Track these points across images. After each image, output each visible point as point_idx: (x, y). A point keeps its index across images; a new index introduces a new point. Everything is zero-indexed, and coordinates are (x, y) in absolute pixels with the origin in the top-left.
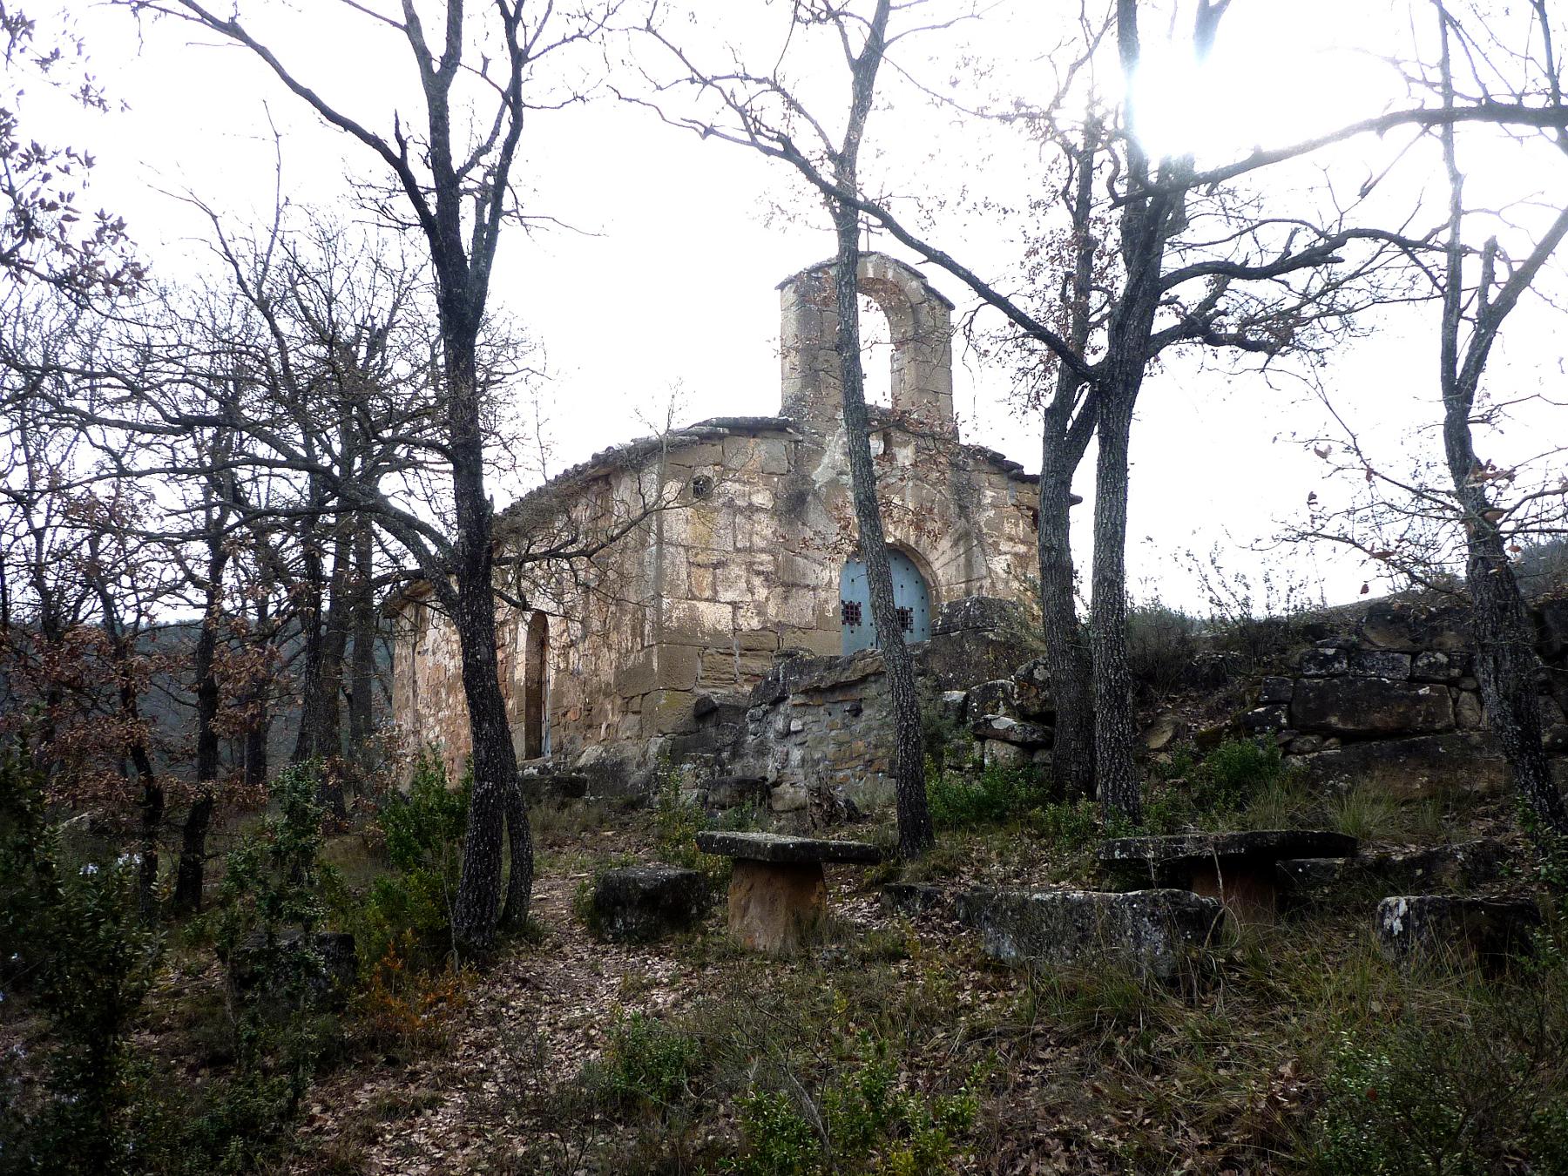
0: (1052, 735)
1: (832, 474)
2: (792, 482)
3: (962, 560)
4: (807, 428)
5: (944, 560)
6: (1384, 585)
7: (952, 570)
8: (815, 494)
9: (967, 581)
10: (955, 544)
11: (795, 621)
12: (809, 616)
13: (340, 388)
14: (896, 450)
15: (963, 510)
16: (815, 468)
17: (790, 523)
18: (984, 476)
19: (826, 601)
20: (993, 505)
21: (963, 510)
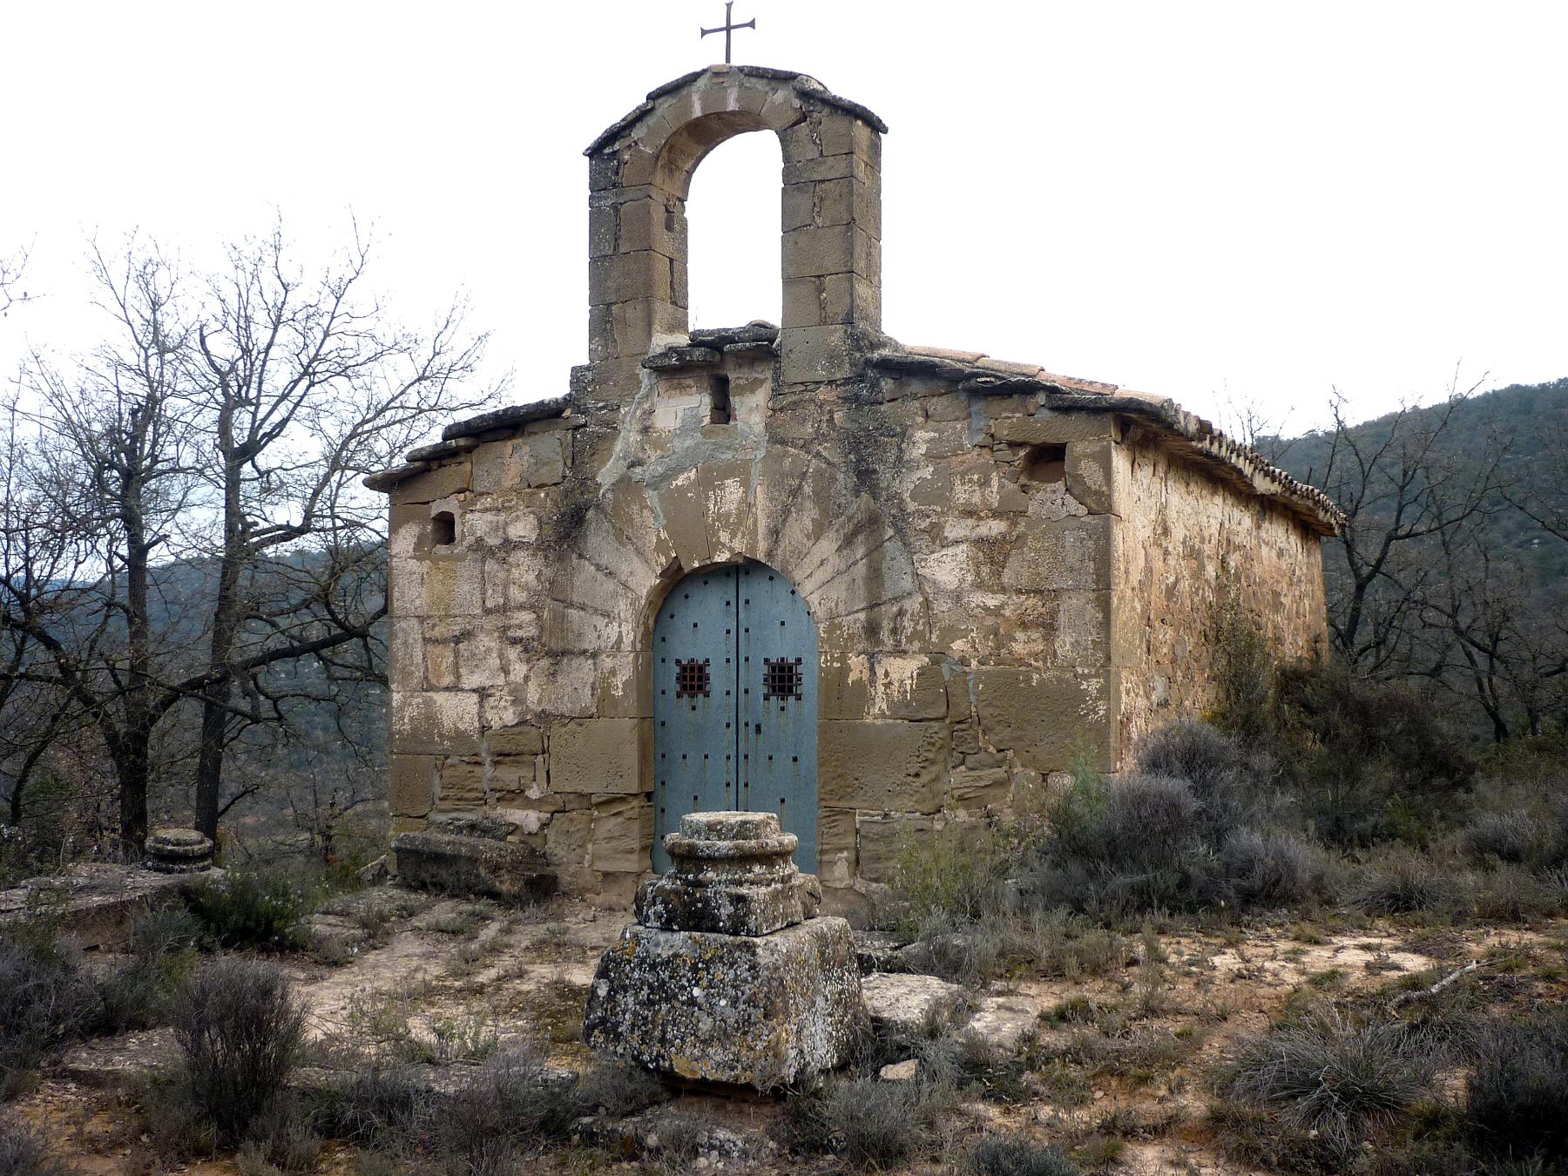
3: (861, 569)
4: (591, 403)
5: (822, 575)
7: (838, 592)
10: (848, 541)
11: (566, 708)
12: (586, 699)
14: (735, 400)
15: (865, 477)
16: (604, 463)
17: (561, 559)
20: (930, 456)
21: (865, 477)
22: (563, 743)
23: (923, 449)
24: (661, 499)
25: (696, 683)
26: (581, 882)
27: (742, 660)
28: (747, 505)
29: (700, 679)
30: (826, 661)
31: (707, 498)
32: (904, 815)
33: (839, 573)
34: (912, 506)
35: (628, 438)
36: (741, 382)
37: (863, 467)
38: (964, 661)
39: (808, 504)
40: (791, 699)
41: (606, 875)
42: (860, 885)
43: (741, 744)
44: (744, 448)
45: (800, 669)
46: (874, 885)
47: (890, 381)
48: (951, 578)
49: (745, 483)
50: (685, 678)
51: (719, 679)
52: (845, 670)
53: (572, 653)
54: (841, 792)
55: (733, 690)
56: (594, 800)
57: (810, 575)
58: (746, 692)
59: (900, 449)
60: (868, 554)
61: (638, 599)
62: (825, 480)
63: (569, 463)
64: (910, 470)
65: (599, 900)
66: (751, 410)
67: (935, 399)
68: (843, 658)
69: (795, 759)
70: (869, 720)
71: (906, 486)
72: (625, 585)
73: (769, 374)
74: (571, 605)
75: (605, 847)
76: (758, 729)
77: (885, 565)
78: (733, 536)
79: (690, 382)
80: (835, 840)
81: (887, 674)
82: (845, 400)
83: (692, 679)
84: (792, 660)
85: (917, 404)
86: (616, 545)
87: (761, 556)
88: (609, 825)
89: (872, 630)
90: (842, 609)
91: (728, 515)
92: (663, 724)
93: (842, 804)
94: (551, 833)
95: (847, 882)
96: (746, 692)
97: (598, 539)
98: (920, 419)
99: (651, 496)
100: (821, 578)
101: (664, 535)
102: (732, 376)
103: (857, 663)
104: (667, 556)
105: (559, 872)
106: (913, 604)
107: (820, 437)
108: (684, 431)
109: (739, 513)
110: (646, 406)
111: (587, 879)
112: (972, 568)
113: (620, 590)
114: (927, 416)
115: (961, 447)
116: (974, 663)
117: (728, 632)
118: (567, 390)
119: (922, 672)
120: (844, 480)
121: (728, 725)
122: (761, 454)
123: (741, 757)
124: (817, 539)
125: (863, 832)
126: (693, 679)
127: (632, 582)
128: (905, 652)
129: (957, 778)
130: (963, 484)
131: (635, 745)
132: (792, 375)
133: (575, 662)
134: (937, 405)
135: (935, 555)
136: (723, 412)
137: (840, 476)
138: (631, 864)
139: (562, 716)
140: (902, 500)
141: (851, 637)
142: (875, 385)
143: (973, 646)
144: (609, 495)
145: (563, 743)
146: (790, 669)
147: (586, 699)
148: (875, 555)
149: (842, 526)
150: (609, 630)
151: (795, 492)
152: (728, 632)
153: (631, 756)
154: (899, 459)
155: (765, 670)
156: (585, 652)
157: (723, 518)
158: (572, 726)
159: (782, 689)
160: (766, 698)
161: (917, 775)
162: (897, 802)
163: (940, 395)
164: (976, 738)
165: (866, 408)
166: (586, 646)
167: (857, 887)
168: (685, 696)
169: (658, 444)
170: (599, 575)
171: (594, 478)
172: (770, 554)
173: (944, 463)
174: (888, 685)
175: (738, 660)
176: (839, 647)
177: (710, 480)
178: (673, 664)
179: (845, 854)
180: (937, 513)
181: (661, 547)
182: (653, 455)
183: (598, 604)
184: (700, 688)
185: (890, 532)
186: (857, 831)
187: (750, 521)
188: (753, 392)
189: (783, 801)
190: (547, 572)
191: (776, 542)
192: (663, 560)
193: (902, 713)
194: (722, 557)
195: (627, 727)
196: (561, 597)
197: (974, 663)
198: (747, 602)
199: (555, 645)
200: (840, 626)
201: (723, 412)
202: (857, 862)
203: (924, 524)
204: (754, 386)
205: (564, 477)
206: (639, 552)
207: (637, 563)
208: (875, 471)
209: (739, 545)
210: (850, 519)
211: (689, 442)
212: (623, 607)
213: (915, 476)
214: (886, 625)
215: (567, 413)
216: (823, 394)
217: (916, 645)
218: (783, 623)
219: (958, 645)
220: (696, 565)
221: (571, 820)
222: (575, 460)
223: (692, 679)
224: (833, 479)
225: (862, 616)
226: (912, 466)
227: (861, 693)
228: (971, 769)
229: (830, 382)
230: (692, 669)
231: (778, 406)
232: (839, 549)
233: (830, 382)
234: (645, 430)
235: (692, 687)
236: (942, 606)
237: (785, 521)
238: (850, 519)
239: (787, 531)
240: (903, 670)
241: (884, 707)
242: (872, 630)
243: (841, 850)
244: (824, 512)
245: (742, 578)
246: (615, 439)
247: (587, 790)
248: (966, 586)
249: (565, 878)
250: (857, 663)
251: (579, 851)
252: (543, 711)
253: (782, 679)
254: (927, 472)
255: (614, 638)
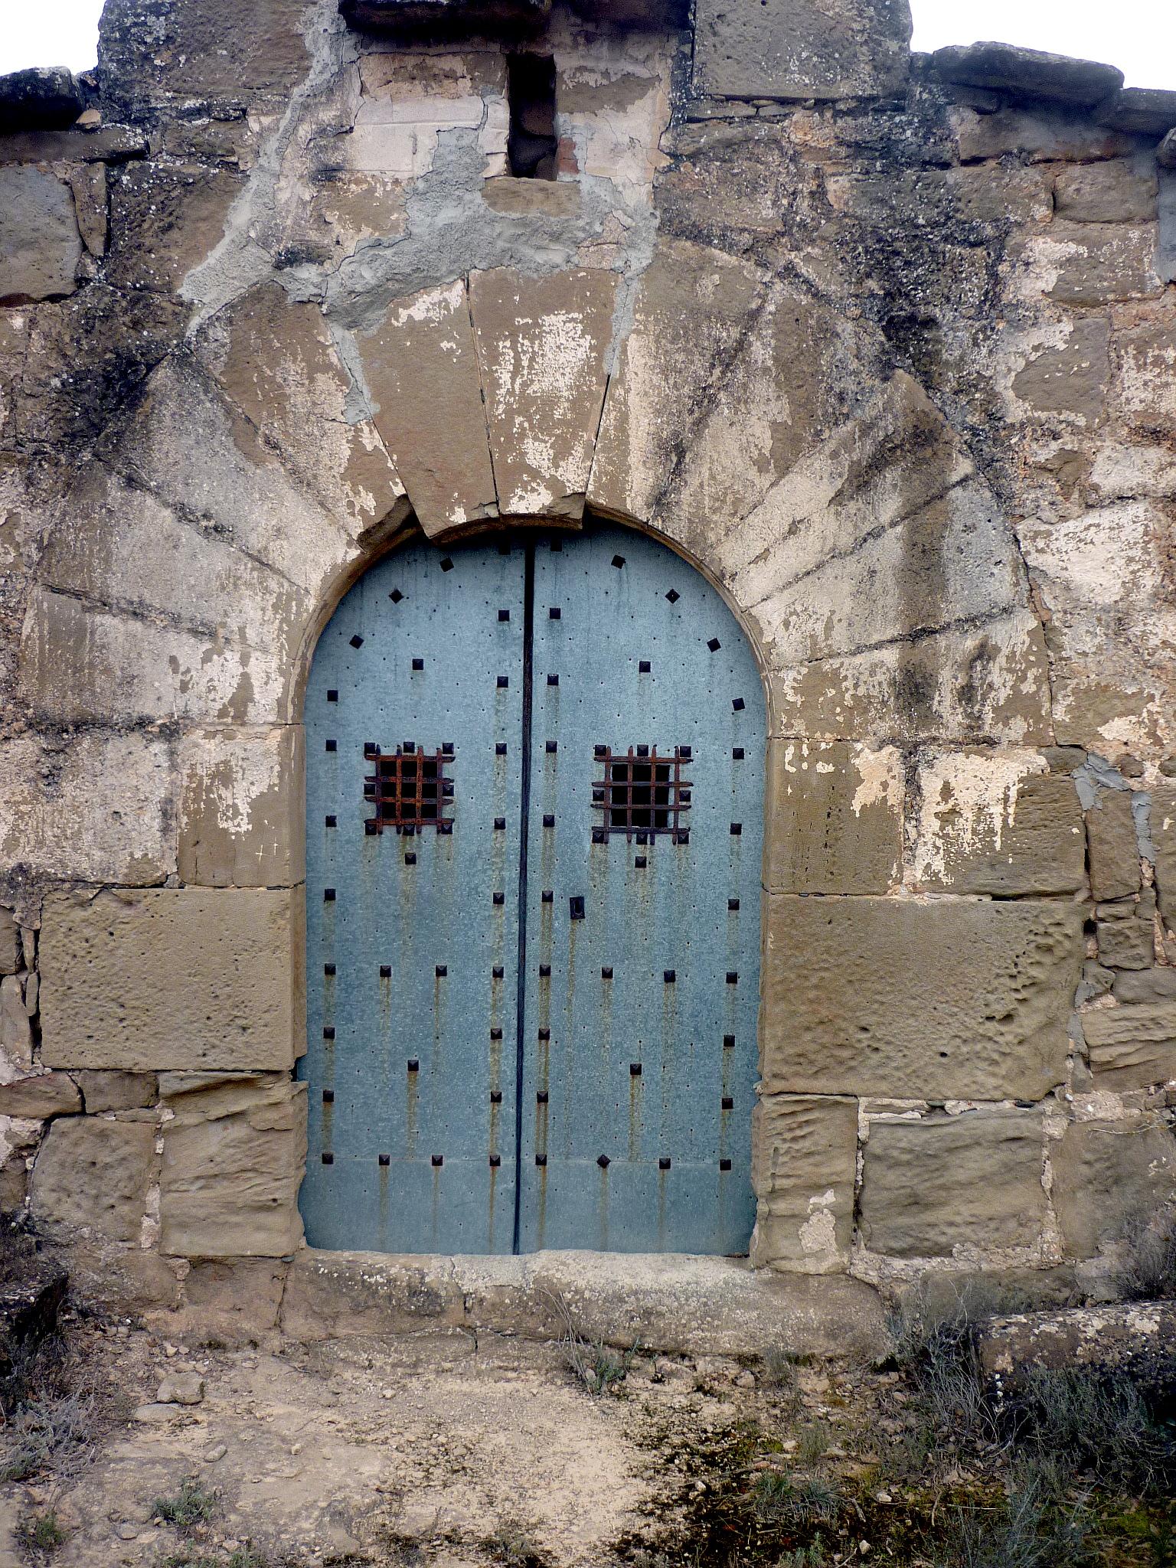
0: (278, 267)
1: (257, 265)
2: (89, 323)
3: (891, 549)
4: (161, 97)
5: (792, 557)
6: (151, 386)
7: (834, 597)
8: (184, 360)
9: (914, 636)
10: (861, 482)
11: (87, 861)
12: (147, 840)
13: (132, 363)
14: (570, 123)
15: (905, 332)
16: (197, 253)
17: (73, 487)
18: (1030, 177)
19: (224, 775)
20: (1069, 299)
21: (905, 332)
22: (79, 947)
23: (1049, 280)
24: (366, 349)
25: (418, 801)
26: (133, 1284)
27: (538, 751)
28: (601, 382)
29: (429, 791)
30: (799, 758)
31: (494, 357)
32: (979, 1104)
33: (836, 554)
34: (1016, 411)
35: (274, 189)
36: (591, 79)
37: (901, 309)
38: (1128, 766)
39: (763, 388)
40: (664, 841)
41: (199, 1263)
42: (865, 1265)
43: (533, 945)
44: (597, 240)
45: (687, 773)
46: (899, 1264)
47: (972, 117)
48: (1104, 578)
49: (599, 328)
50: (389, 790)
51: (477, 791)
52: (845, 781)
53: (104, 724)
54: (821, 1059)
55: (513, 818)
56: (168, 1085)
57: (764, 556)
58: (549, 822)
59: (994, 277)
60: (910, 514)
61: (299, 594)
62: (806, 333)
63: (97, 245)
64: (1017, 325)
65: (178, 1323)
66: (616, 151)
67: (1076, 170)
68: (841, 753)
69: (670, 977)
70: (900, 895)
71: (1005, 362)
72: (261, 562)
73: (663, 68)
74: (105, 605)
75: (196, 1199)
76: (577, 908)
77: (949, 541)
78: (561, 452)
79: (456, 64)
80: (805, 1167)
81: (947, 792)
82: (858, 148)
83: (409, 790)
84: (665, 751)
85: (1033, 174)
86: (235, 458)
87: (636, 504)
88: (209, 1144)
89: (914, 689)
90: (840, 638)
91: (550, 401)
92: (330, 895)
93: (822, 1084)
94: (45, 1170)
95: (834, 1259)
96: (549, 822)
97: (180, 436)
98: (1041, 211)
99: (340, 343)
100: (796, 557)
101: (371, 440)
102: (565, 62)
103: (876, 771)
104: (379, 492)
105: (68, 1262)
106: (1014, 634)
107: (789, 229)
108: (437, 184)
109: (579, 397)
110: (327, 115)
111: (152, 1276)
112: (1155, 558)
113: (246, 570)
114: (1056, 207)
115: (1140, 283)
116: (1151, 772)
117: (503, 683)
118: (96, 64)
119: (1030, 789)
120: (855, 338)
121: (499, 900)
122: (640, 258)
123: (532, 974)
124: (784, 470)
125: (875, 1147)
126: (409, 790)
127: (281, 554)
128: (991, 742)
129: (1101, 1021)
130: (1140, 368)
131: (286, 956)
132: (723, 74)
133: (115, 748)
134: (1079, 183)
135: (1070, 526)
136: (534, 151)
137: (846, 328)
138: (276, 1235)
139: (78, 881)
140: (992, 396)
141: (862, 705)
142: (932, 123)
143: (1152, 734)
144: (220, 333)
145: (79, 947)
146: (663, 771)
147: (147, 840)
148: (927, 516)
149: (847, 444)
150: (213, 669)
151: (729, 357)
152: (503, 683)
153: (273, 981)
154: (991, 299)
155: (598, 772)
156: (143, 723)
157: (537, 409)
158: (105, 904)
159: (641, 818)
160: (599, 837)
161: (1008, 1018)
162: (962, 1079)
163: (1089, 161)
164: (1147, 936)
165: (910, 174)
166: (145, 707)
167: (858, 1270)
168: (389, 831)
169: (361, 213)
170: (187, 533)
171: (169, 288)
172: (660, 500)
173: (1094, 317)
174: (948, 817)
175: (526, 749)
176: (833, 727)
177: (503, 310)
178: (357, 755)
179: (830, 1197)
180: (1075, 430)
181: (362, 468)
182: (353, 239)
183: (182, 602)
184: (431, 813)
185: (964, 466)
186: (862, 1145)
187: (609, 420)
188: (621, 106)
189: (636, 1071)
190: (34, 519)
191: (678, 471)
192: (368, 501)
193: (986, 878)
194: (529, 502)
195: (261, 910)
196: (75, 583)
197: (1151, 772)
198: (555, 614)
199: (58, 702)
200: (835, 679)
201: (534, 151)
202: (857, 1213)
203: (1045, 452)
204: (623, 92)
205: (81, 281)
206: (302, 480)
207: (294, 508)
208: (930, 323)
209: (574, 475)
210: (866, 429)
211: (450, 214)
212: (253, 614)
213: (1036, 337)
214: (948, 680)
215: (91, 117)
216: (803, 129)
217: (1019, 727)
218: (645, 667)
219: (1117, 731)
220: (459, 517)
221: (103, 1135)
222: (115, 239)
223: (409, 790)
224: (827, 334)
225: (890, 657)
226: (1022, 319)
227: (886, 834)
228: (1125, 1002)
229: (821, 104)
230: (409, 767)
231: (686, 149)
232: (838, 499)
233: (821, 104)
234: (327, 175)
235: (408, 811)
236: (1081, 640)
237: (700, 424)
238: (866, 429)
239: (706, 446)
240: (985, 784)
241: (938, 865)
242: (914, 689)
243: (819, 1188)
244: (803, 408)
245: (543, 561)
246: (232, 194)
247: (146, 1063)
248: (1141, 597)
249: (86, 1278)
250: (876, 771)
251: (124, 1209)
252: (21, 869)
253: (641, 795)
254: (1057, 334)
255: (227, 689)
